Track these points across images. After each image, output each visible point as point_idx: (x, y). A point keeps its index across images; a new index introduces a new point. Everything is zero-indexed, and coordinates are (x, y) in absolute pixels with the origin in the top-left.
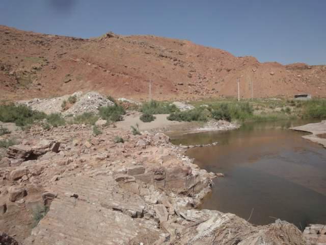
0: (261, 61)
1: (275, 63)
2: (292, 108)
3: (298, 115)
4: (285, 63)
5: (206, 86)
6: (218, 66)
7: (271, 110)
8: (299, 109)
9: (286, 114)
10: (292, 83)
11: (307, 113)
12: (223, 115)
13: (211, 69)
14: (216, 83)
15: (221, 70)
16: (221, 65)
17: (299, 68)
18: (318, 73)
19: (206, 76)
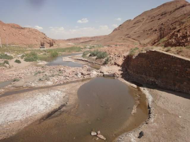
18: (28, 32)
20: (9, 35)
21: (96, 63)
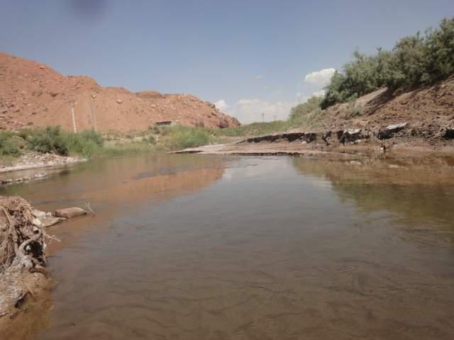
0: (103, 84)
1: (122, 88)
2: (157, 137)
3: (165, 145)
4: (134, 90)
5: (16, 118)
6: (35, 87)
7: (129, 141)
8: (166, 137)
9: (150, 144)
10: (145, 114)
11: (177, 142)
12: (52, 144)
13: (23, 92)
14: (33, 114)
15: (41, 93)
16: (41, 86)
17: (151, 96)
18: (174, 103)
19: (14, 103)
20: (127, 112)
21: (385, 135)
